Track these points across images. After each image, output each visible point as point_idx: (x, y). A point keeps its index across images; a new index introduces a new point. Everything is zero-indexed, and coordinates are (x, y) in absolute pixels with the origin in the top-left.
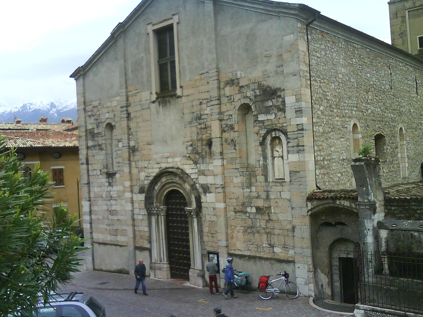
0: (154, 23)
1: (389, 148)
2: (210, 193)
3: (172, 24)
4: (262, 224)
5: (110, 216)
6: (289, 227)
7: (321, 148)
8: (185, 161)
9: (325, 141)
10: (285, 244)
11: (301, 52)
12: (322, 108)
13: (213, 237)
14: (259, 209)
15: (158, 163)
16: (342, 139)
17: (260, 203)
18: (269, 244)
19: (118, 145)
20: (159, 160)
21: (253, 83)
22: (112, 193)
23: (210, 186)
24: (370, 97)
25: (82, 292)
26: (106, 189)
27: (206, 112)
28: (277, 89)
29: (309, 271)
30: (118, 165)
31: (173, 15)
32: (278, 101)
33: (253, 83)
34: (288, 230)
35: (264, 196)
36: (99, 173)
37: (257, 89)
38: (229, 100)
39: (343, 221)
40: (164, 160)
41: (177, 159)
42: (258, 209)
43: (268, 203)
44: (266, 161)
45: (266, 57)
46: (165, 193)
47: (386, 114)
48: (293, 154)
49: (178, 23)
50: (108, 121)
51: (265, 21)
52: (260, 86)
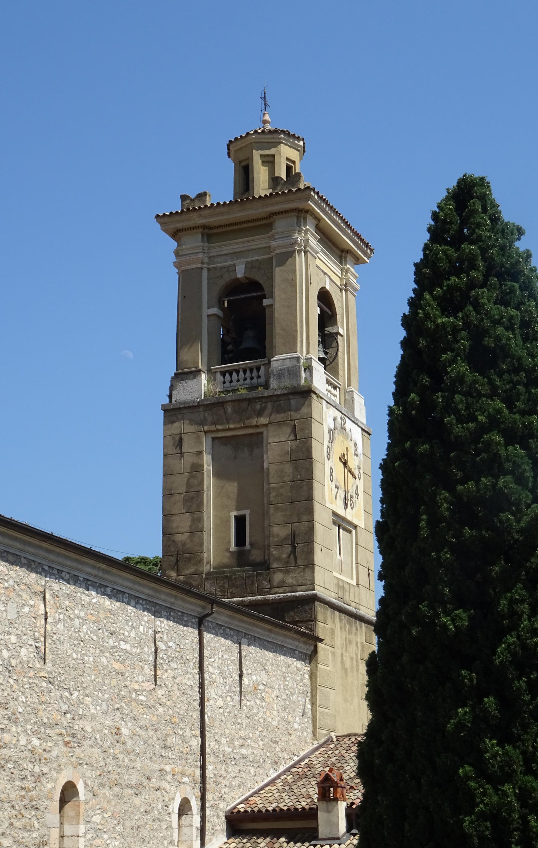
10: (171, 515)
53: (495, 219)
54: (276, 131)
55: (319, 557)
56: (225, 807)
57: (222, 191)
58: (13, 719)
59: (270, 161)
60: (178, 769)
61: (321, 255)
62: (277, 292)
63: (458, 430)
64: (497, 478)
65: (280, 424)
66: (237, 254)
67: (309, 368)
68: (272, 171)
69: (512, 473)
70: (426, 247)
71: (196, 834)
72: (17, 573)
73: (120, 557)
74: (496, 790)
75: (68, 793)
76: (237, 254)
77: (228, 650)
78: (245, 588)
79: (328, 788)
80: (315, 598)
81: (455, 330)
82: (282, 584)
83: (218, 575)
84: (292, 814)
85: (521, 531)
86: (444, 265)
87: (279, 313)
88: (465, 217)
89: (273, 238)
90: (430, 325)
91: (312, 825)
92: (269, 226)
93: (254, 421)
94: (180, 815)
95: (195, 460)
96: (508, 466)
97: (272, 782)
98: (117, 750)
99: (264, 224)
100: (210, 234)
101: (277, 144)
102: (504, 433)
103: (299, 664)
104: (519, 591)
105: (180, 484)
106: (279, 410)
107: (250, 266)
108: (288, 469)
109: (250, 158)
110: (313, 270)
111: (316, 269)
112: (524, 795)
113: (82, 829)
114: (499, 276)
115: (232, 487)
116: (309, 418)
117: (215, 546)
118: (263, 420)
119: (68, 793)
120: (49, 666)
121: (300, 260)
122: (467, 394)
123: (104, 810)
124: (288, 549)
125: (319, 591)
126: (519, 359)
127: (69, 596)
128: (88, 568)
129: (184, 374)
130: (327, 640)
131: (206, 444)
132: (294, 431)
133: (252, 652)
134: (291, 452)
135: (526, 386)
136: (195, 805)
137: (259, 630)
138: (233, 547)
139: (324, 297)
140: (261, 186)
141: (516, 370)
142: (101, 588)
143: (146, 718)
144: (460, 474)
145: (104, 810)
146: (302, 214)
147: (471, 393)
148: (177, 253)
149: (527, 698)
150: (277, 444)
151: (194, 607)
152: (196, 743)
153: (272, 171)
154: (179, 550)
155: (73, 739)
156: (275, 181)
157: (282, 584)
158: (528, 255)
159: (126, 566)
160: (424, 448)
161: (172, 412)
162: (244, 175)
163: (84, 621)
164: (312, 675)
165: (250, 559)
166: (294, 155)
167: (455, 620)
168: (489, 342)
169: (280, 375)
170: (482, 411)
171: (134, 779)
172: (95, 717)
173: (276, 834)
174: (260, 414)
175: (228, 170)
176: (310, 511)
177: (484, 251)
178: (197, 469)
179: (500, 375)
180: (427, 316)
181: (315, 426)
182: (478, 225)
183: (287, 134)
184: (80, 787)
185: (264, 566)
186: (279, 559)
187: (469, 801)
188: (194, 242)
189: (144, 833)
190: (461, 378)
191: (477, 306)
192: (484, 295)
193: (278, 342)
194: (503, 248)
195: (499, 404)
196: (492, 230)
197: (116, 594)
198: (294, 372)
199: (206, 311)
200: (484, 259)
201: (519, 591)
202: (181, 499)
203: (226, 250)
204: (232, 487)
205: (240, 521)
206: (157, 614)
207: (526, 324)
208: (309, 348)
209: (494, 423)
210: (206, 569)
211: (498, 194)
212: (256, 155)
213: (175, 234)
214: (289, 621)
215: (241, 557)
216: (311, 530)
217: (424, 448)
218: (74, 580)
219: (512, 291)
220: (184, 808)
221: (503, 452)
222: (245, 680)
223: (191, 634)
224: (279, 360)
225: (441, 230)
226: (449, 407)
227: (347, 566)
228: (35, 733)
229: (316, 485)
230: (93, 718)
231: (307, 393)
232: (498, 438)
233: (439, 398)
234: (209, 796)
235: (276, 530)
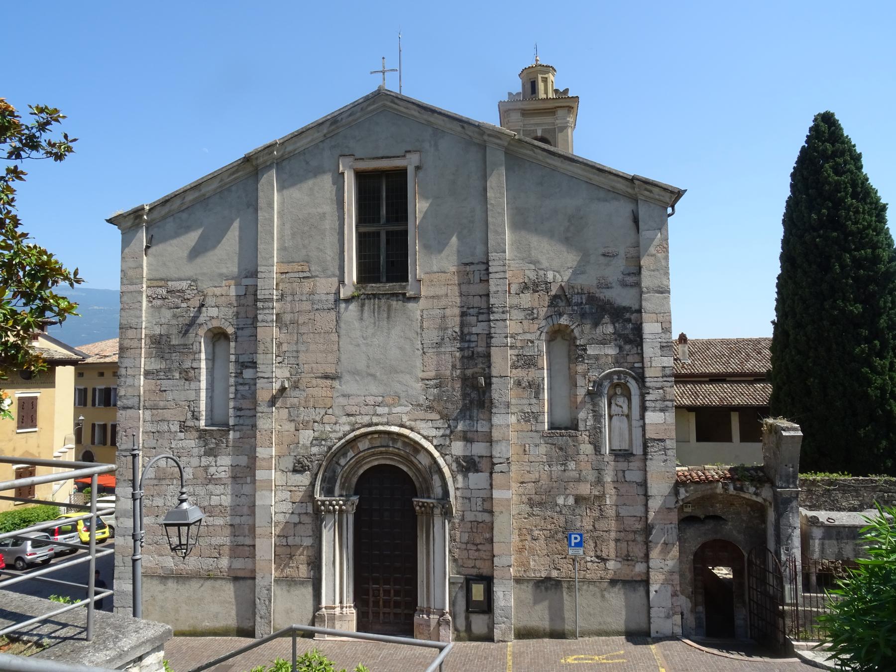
0: (358, 156)
2: (477, 471)
4: (584, 524)
6: (638, 526)
8: (421, 414)
10: (628, 555)
13: (478, 550)
15: (348, 415)
17: (585, 489)
19: (242, 373)
21: (578, 293)
22: (212, 470)
23: (477, 459)
27: (474, 330)
28: (624, 308)
30: (239, 413)
31: (407, 152)
32: (625, 328)
33: (578, 293)
34: (635, 532)
35: (591, 476)
37: (586, 304)
38: (529, 315)
39: (719, 513)
40: (370, 410)
41: (402, 411)
42: (579, 499)
43: (599, 488)
44: (600, 422)
45: (604, 255)
46: (361, 471)
48: (653, 411)
49: (418, 168)
50: (215, 323)
51: (605, 200)
66: (538, 125)
76: (538, 125)
88: (826, 169)
91: (464, 288)
101: (548, 72)
107: (544, 131)
187: (869, 383)
203: (532, 122)
212: (540, 76)
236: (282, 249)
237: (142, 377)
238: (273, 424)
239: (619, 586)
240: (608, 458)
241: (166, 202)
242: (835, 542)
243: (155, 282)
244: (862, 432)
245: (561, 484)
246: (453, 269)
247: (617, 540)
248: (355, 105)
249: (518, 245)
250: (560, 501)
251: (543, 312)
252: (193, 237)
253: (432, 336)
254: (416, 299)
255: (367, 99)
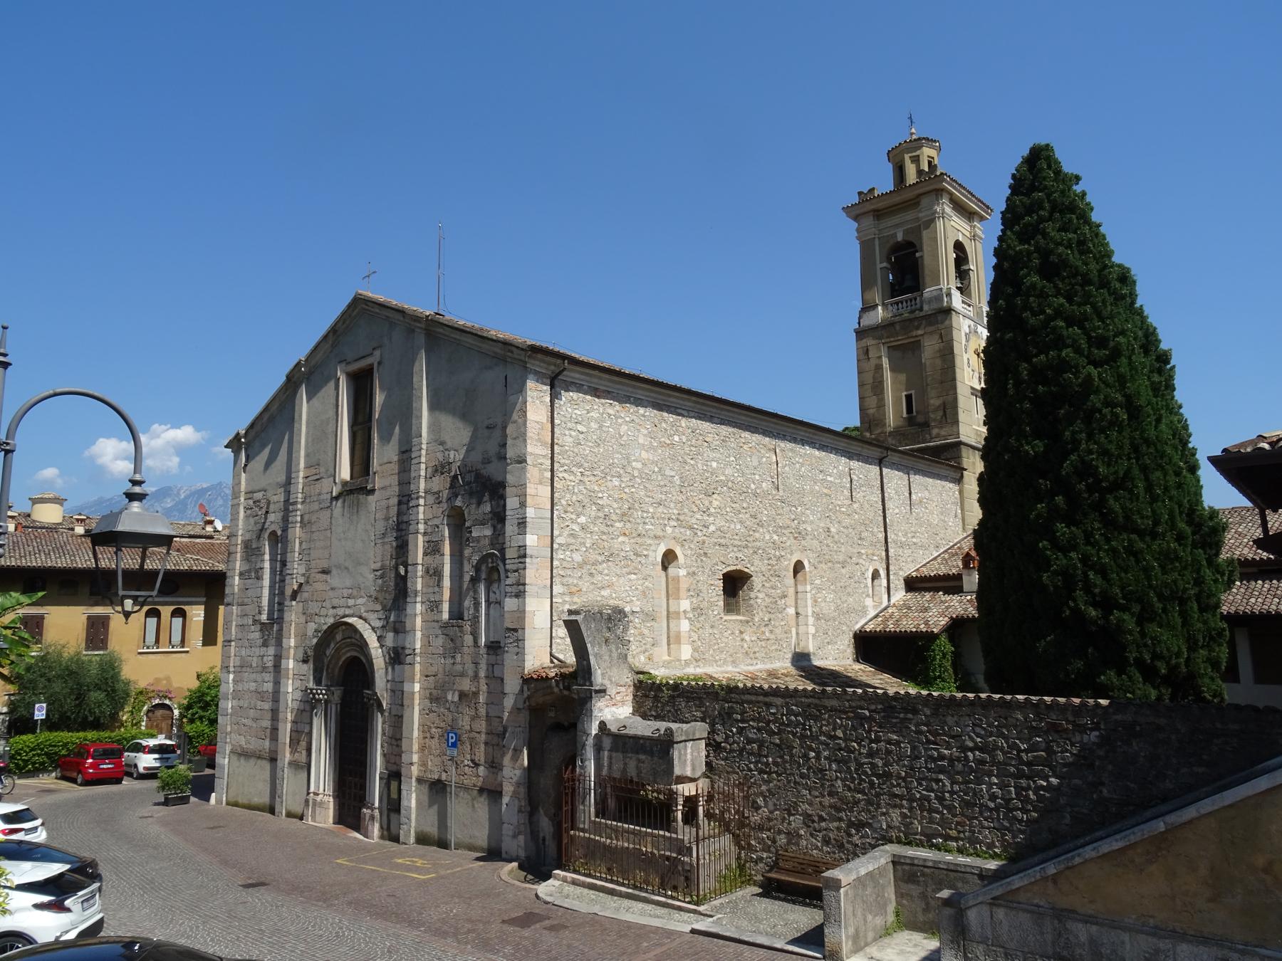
1: (761, 595)
3: (372, 365)
5: (259, 703)
7: (574, 589)
9: (587, 578)
11: (534, 425)
12: (582, 520)
14: (462, 695)
15: (334, 608)
16: (633, 577)
18: (472, 761)
20: (336, 602)
24: (716, 503)
25: (262, 880)
26: (258, 651)
29: (520, 811)
36: (250, 622)
47: (757, 535)
52: (478, 475)
53: (1058, 172)
54: (919, 139)
55: (962, 417)
56: (904, 574)
57: (884, 183)
58: (760, 524)
59: (916, 160)
60: (870, 552)
61: (955, 218)
62: (925, 247)
63: (1032, 321)
64: (1061, 350)
65: (931, 333)
66: (897, 226)
67: (949, 295)
68: (918, 166)
69: (1072, 346)
70: (1008, 199)
71: (884, 591)
72: (757, 438)
73: (839, 429)
74: (1066, 556)
75: (798, 567)
76: (897, 226)
77: (901, 478)
78: (903, 438)
79: (967, 559)
80: (961, 443)
81: (1029, 253)
82: (938, 436)
83: (897, 433)
84: (946, 577)
85: (1080, 385)
86: (1020, 210)
87: (927, 261)
89: (920, 211)
90: (1011, 252)
92: (918, 204)
93: (914, 333)
94: (873, 579)
95: (877, 361)
96: (1069, 341)
97: (935, 559)
98: (829, 541)
99: (914, 203)
100: (879, 214)
102: (1065, 320)
103: (951, 485)
104: (1078, 425)
105: (869, 378)
106: (931, 324)
107: (906, 232)
108: (938, 362)
109: (903, 160)
110: (949, 229)
111: (952, 227)
112: (1085, 560)
113: (808, 588)
114: (1061, 212)
115: (903, 377)
116: (950, 327)
117: (893, 415)
118: (920, 332)
119: (798, 567)
120: (781, 493)
121: (940, 224)
122: (1038, 297)
123: (822, 577)
124: (940, 413)
125: (963, 438)
126: (1076, 267)
127: (791, 450)
128: (802, 433)
129: (867, 308)
130: (970, 468)
131: (884, 351)
132: (941, 337)
133: (917, 479)
134: (940, 351)
135: (1082, 286)
136: (883, 573)
137: (921, 465)
138: (905, 415)
139: (959, 246)
140: (911, 176)
141: (1074, 276)
142: (812, 444)
143: (847, 521)
144: (1035, 351)
145: (822, 577)
146: (939, 192)
147: (1042, 295)
148: (858, 230)
149: (1086, 495)
150: (930, 346)
151: (876, 452)
152: (882, 536)
153: (918, 166)
154: (870, 419)
155: (799, 535)
156: (920, 172)
157: (938, 436)
158: (1084, 194)
159: (845, 435)
160: (1009, 336)
161: (861, 333)
162: (900, 171)
163: (802, 465)
164: (961, 492)
165: (916, 422)
166: (933, 153)
167: (1032, 448)
168: (1053, 258)
169: (930, 301)
170: (1049, 306)
171: (841, 558)
172: (813, 521)
173: (937, 590)
174: (917, 328)
175: (889, 168)
176: (955, 388)
177: (1048, 196)
178: (879, 368)
179: (1063, 280)
180: (1009, 246)
181: (955, 333)
182: (1044, 178)
183: (927, 139)
184: (678, 551)
185: (926, 425)
186: (935, 420)
187: (1047, 563)
188: (869, 221)
189: (849, 590)
190: (1033, 286)
191: (1045, 235)
192: (1050, 228)
193: (928, 280)
194: (1063, 192)
195: (1062, 300)
196: (1055, 180)
197: (822, 448)
198: (939, 298)
199: (879, 266)
200: (1049, 201)
201: (1078, 425)
202: (870, 387)
204: (903, 377)
205: (909, 398)
206: (850, 458)
207: (1081, 243)
208: (948, 279)
209: (1058, 313)
210: (888, 429)
211: (1059, 154)
212: (907, 157)
213: (856, 218)
214: (943, 459)
215: (911, 420)
216: (955, 400)
217: (1009, 336)
218: (794, 440)
219: (1070, 220)
220: (875, 575)
221: (1065, 333)
222: (914, 497)
223: (875, 469)
224: (928, 291)
225: (1018, 186)
226: (1026, 307)
227: (972, 423)
228: (775, 532)
229: (958, 370)
230: (812, 522)
231: (949, 311)
232: (1062, 324)
233: (1019, 301)
234: (891, 568)
235: (932, 402)
236: (307, 455)
237: (237, 578)
238: (293, 615)
239: (485, 795)
240: (483, 651)
241: (252, 425)
242: (621, 756)
243: (250, 493)
244: (1041, 645)
245: (452, 675)
246: (396, 458)
247: (486, 744)
248: (344, 314)
249: (434, 427)
250: (449, 697)
251: (445, 494)
252: (267, 451)
253: (381, 526)
254: (372, 491)
255: (349, 306)
